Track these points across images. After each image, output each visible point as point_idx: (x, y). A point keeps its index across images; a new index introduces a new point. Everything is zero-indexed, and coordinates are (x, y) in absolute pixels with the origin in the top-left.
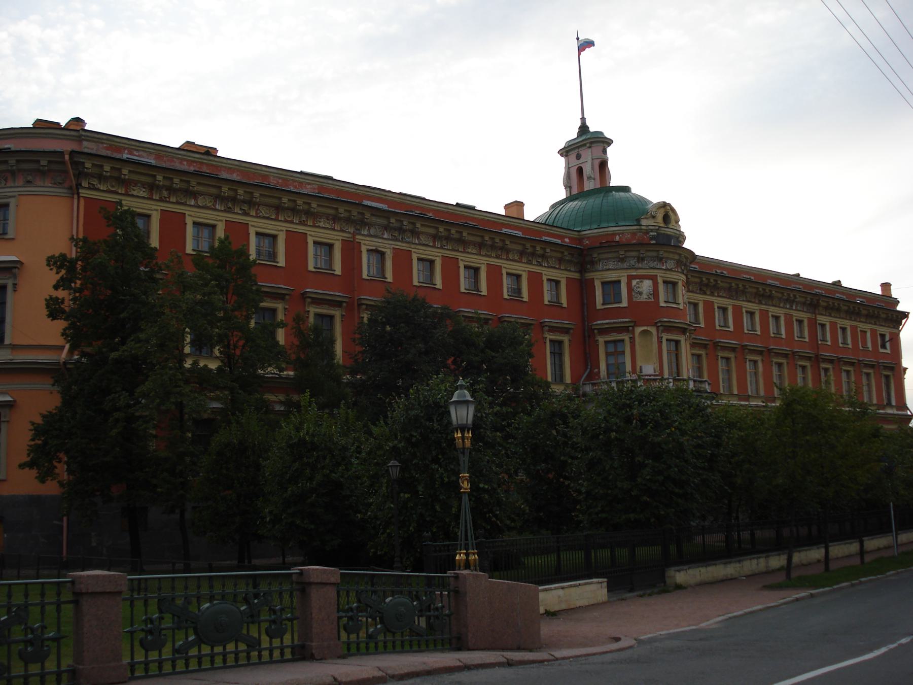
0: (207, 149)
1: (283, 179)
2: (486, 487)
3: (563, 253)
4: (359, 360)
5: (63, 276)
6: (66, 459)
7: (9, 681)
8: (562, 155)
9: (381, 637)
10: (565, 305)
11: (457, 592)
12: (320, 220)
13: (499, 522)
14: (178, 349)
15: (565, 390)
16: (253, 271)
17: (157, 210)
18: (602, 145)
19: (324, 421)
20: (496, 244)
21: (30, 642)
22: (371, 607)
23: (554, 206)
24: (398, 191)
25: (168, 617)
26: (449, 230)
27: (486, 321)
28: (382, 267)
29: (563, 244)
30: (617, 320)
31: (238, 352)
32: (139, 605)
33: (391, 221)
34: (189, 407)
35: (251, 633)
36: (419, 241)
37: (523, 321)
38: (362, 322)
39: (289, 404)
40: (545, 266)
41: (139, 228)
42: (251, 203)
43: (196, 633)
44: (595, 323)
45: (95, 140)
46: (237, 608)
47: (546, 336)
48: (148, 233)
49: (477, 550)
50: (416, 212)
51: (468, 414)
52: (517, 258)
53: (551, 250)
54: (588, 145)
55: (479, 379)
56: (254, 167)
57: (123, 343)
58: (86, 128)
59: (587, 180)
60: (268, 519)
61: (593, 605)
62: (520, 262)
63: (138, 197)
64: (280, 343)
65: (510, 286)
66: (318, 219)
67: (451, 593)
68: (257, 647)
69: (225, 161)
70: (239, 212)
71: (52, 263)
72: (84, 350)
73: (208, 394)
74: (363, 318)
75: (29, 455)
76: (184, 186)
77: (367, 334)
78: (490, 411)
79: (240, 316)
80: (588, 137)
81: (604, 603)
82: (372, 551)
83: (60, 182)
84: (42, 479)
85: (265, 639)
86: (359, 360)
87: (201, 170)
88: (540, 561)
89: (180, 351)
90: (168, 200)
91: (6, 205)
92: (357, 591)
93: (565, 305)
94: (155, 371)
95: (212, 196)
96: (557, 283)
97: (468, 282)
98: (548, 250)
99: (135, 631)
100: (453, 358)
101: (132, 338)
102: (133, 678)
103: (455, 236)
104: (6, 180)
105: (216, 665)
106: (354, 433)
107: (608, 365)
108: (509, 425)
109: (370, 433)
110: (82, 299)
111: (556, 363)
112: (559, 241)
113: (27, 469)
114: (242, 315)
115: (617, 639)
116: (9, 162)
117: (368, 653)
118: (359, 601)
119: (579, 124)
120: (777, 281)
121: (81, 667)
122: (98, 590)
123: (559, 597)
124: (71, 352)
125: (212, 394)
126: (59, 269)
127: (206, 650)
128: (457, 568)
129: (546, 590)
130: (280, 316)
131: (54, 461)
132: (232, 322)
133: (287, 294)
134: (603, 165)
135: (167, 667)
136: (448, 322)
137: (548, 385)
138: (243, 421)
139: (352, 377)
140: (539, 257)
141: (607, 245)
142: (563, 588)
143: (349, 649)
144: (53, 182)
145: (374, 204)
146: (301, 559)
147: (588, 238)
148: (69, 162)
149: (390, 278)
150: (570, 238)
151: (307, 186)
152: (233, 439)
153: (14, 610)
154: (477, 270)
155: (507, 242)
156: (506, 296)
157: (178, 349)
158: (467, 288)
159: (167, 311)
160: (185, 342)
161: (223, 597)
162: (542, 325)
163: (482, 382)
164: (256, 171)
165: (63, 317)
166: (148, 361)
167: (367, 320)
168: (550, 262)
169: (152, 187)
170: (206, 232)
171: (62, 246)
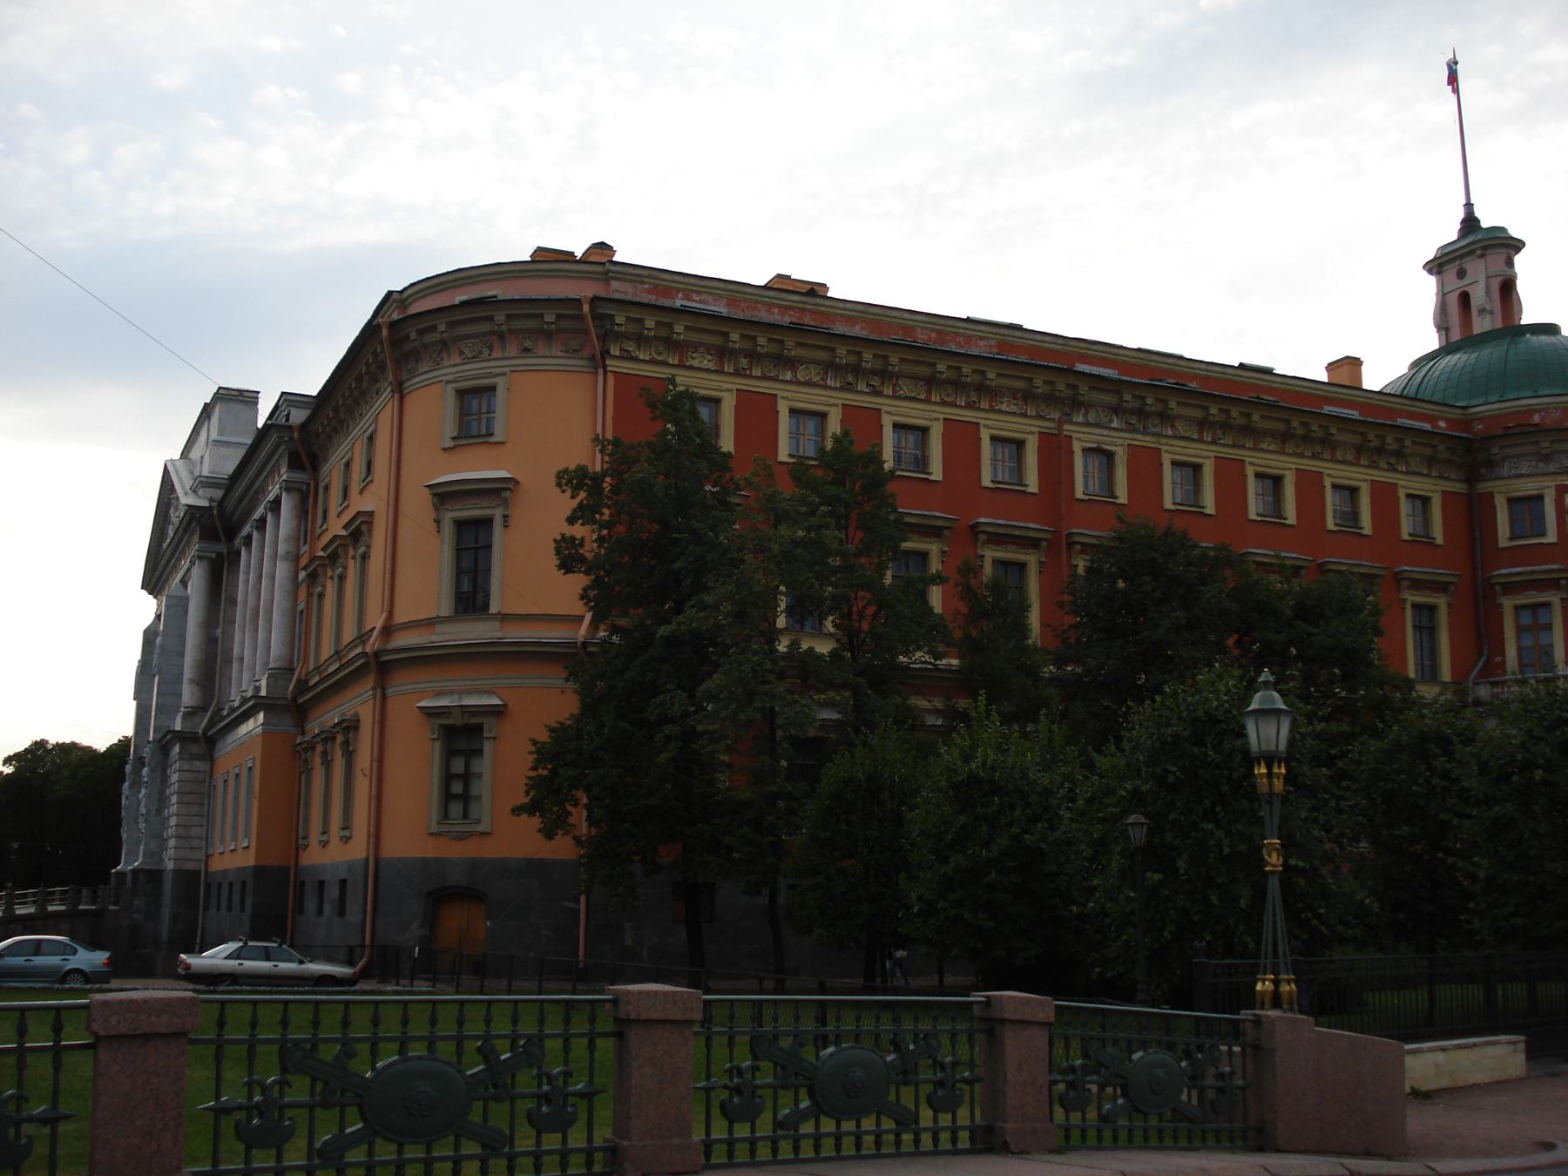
0: (810, 286)
1: (939, 332)
2: (1301, 864)
3: (1434, 447)
4: (1070, 640)
5: (582, 501)
6: (585, 800)
7: (340, 1171)
8: (1430, 272)
9: (1123, 1122)
10: (1440, 540)
11: (1257, 1048)
12: (1001, 400)
13: (1323, 928)
14: (767, 621)
15: (1441, 694)
16: (891, 488)
17: (730, 391)
18: (1505, 251)
19: (1011, 743)
20: (1293, 431)
21: (545, 1098)
22: (1107, 1068)
23: (1417, 364)
24: (1135, 346)
25: (766, 1065)
26: (1228, 412)
27: (1296, 570)
28: (1109, 478)
29: (1435, 430)
30: (1536, 568)
31: (865, 626)
32: (719, 1043)
33: (1125, 399)
34: (785, 716)
35: (903, 1101)
36: (1174, 432)
37: (1362, 570)
38: (1074, 575)
39: (950, 714)
40: (1402, 472)
41: (702, 421)
42: (885, 375)
43: (812, 1097)
44: (1495, 573)
45: (629, 277)
46: (881, 1057)
47: (1405, 597)
48: (717, 428)
49: (1294, 974)
50: (1169, 380)
51: (1278, 733)
52: (1349, 457)
53: (1414, 443)
54: (1478, 252)
55: (1288, 673)
56: (889, 313)
57: (678, 610)
58: (615, 259)
59: (1479, 315)
60: (915, 910)
61: (1499, 1083)
62: (1357, 464)
63: (699, 369)
64: (936, 611)
65: (1338, 508)
66: (690, 353)
67: (1248, 1050)
68: (913, 1126)
69: (841, 305)
70: (867, 390)
71: (564, 481)
72: (615, 623)
73: (815, 697)
74: (1077, 566)
75: (527, 793)
76: (774, 348)
77: (1084, 595)
78: (1309, 730)
79: (868, 565)
80: (1479, 237)
81: (1519, 1080)
82: (1097, 970)
83: (575, 348)
84: (548, 833)
85: (926, 1114)
86: (1070, 640)
87: (802, 322)
88: (1396, 1001)
89: (769, 624)
90: (748, 372)
91: (492, 389)
92: (1083, 1039)
93: (1440, 540)
94: (730, 656)
95: (820, 365)
96: (1425, 501)
97: (1261, 501)
98: (1408, 443)
99: (713, 1089)
100: (1236, 636)
101: (693, 602)
102: (709, 1166)
103: (1238, 422)
104: (491, 348)
105: (863, 1152)
106: (1064, 766)
107: (1520, 650)
108: (1343, 755)
109: (1089, 766)
110: (613, 540)
111: (1424, 644)
112: (1427, 426)
113: (525, 816)
114: (871, 564)
115: (1549, 1147)
116: (496, 318)
117: (1100, 1147)
118: (1086, 1055)
119: (1461, 215)
120: (1354, 409)
121: (625, 1143)
122: (655, 1016)
123: (1437, 1065)
124: (594, 625)
125: (822, 696)
126: (576, 489)
127: (828, 1125)
128: (1258, 1006)
129: (1414, 1052)
130: (935, 566)
131: (567, 805)
132: (856, 575)
133: (947, 528)
134: (1508, 287)
135: (764, 1153)
136: (1228, 573)
137: (1409, 685)
138: (874, 742)
139: (1058, 669)
140: (1392, 454)
141: (1516, 432)
142: (1443, 1050)
143: (1067, 1138)
144: (564, 349)
145: (1096, 370)
146: (970, 980)
147: (1482, 420)
148: (589, 315)
149: (1122, 496)
150: (1448, 420)
151: (978, 342)
152: (857, 771)
153: (522, 1043)
154: (1277, 481)
155: (1333, 430)
156: (1331, 526)
157: (767, 621)
158: (1261, 511)
159: (748, 557)
160: (778, 609)
161: (857, 1038)
162: (1397, 578)
163: (1293, 678)
164: (893, 320)
165: (583, 569)
166: (719, 640)
167: (1085, 571)
168: (1413, 464)
169: (722, 353)
170: (810, 425)
171: (580, 453)
